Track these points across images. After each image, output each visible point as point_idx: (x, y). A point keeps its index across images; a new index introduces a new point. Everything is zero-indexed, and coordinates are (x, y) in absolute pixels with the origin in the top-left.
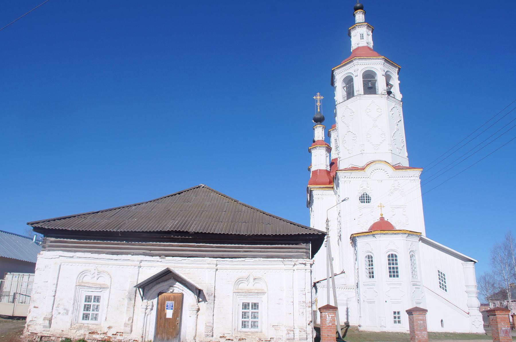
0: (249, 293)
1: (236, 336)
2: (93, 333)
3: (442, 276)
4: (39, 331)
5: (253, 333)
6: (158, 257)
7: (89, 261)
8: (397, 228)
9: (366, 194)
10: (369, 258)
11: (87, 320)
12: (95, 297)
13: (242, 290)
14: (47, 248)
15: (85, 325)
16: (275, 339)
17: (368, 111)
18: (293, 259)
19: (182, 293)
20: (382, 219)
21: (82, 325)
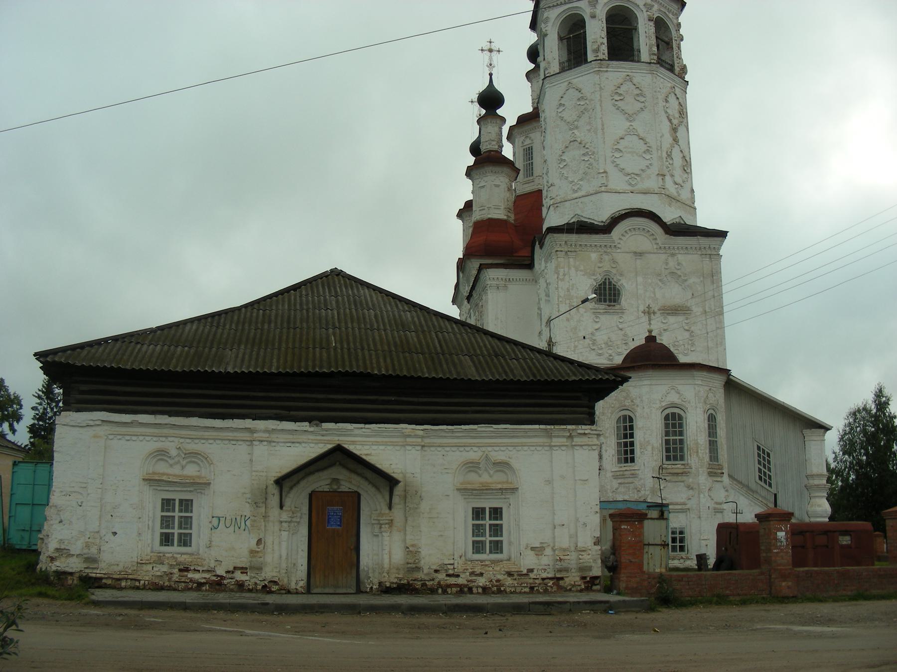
0: (484, 490)
1: (465, 568)
2: (187, 570)
3: (764, 456)
4: (77, 570)
5: (494, 562)
6: (307, 424)
7: (166, 431)
8: (682, 359)
9: (609, 282)
10: (625, 421)
11: (168, 545)
12: (181, 501)
13: (473, 484)
14: (72, 405)
15: (167, 555)
16: (535, 571)
17: (618, 98)
18: (569, 427)
19: (356, 492)
20: (651, 339)
21: (161, 555)
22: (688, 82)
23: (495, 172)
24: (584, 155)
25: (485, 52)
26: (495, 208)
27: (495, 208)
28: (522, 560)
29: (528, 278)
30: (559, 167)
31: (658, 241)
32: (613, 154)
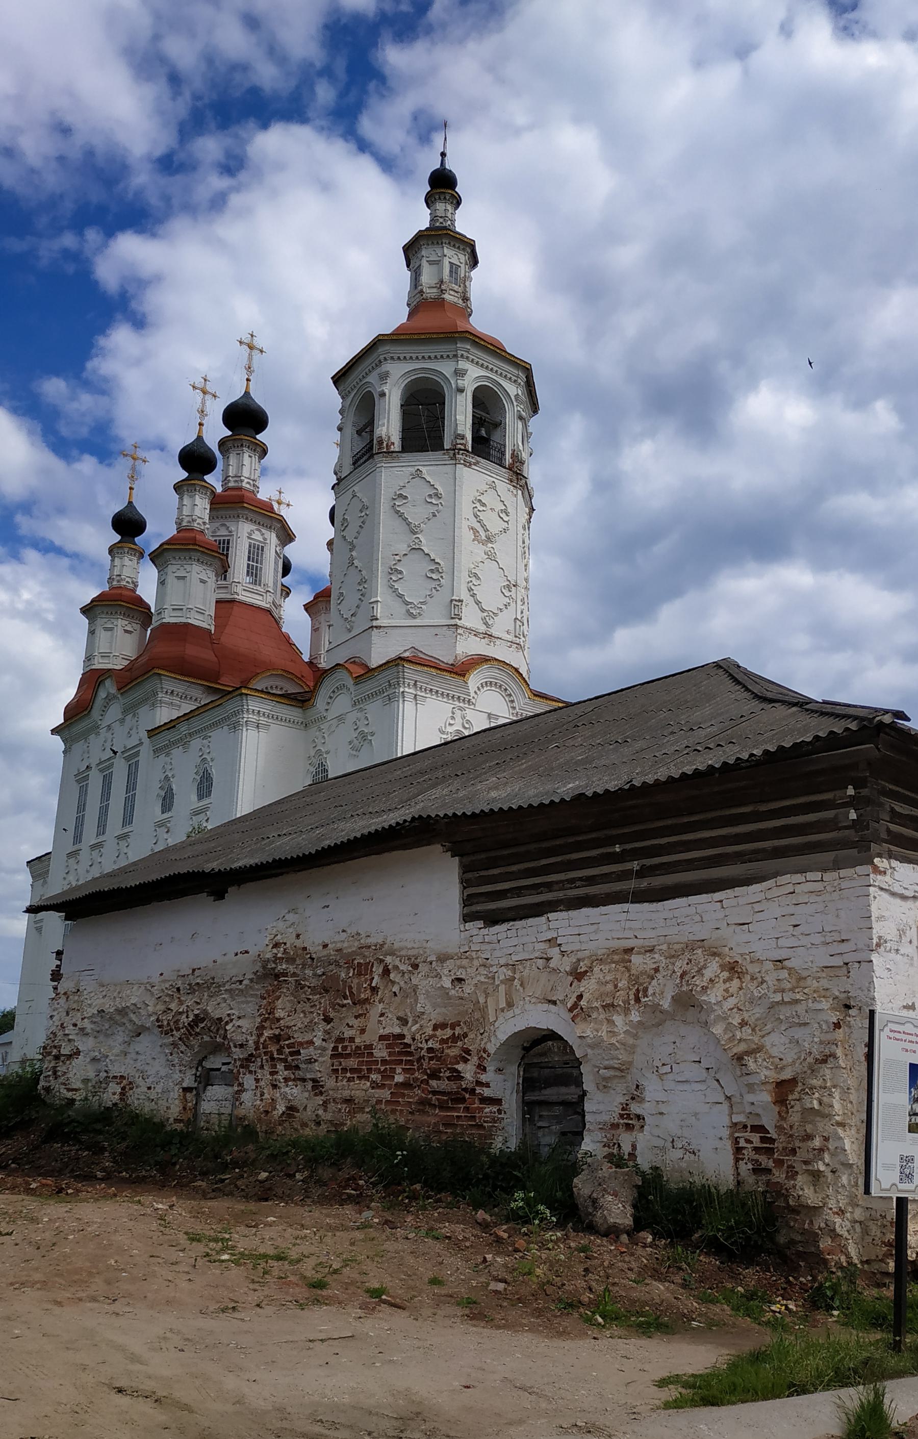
22: (534, 510)
23: (202, 562)
24: (432, 571)
25: (198, 391)
26: (197, 612)
27: (197, 612)
28: (521, 1082)
29: (297, 719)
30: (391, 579)
31: (516, 704)
32: (470, 579)
